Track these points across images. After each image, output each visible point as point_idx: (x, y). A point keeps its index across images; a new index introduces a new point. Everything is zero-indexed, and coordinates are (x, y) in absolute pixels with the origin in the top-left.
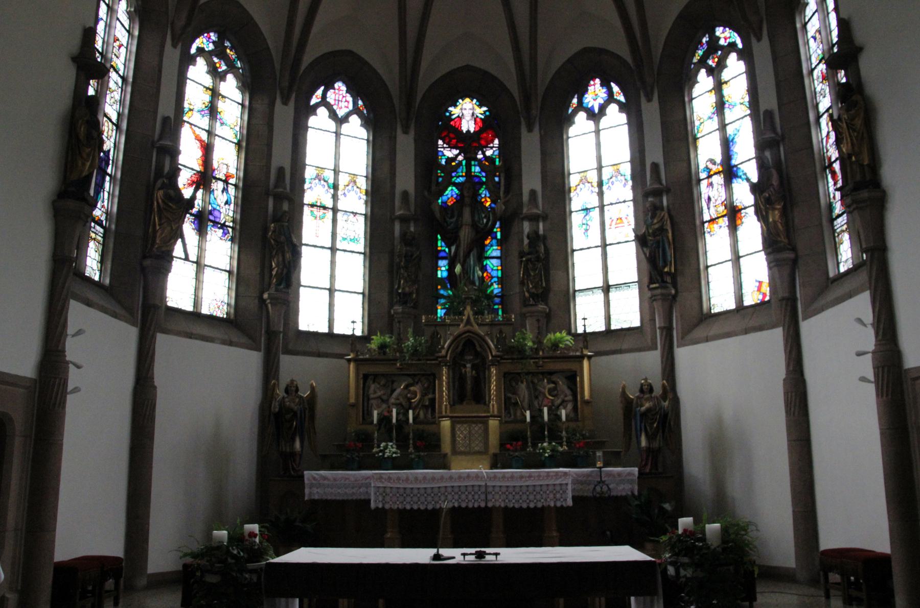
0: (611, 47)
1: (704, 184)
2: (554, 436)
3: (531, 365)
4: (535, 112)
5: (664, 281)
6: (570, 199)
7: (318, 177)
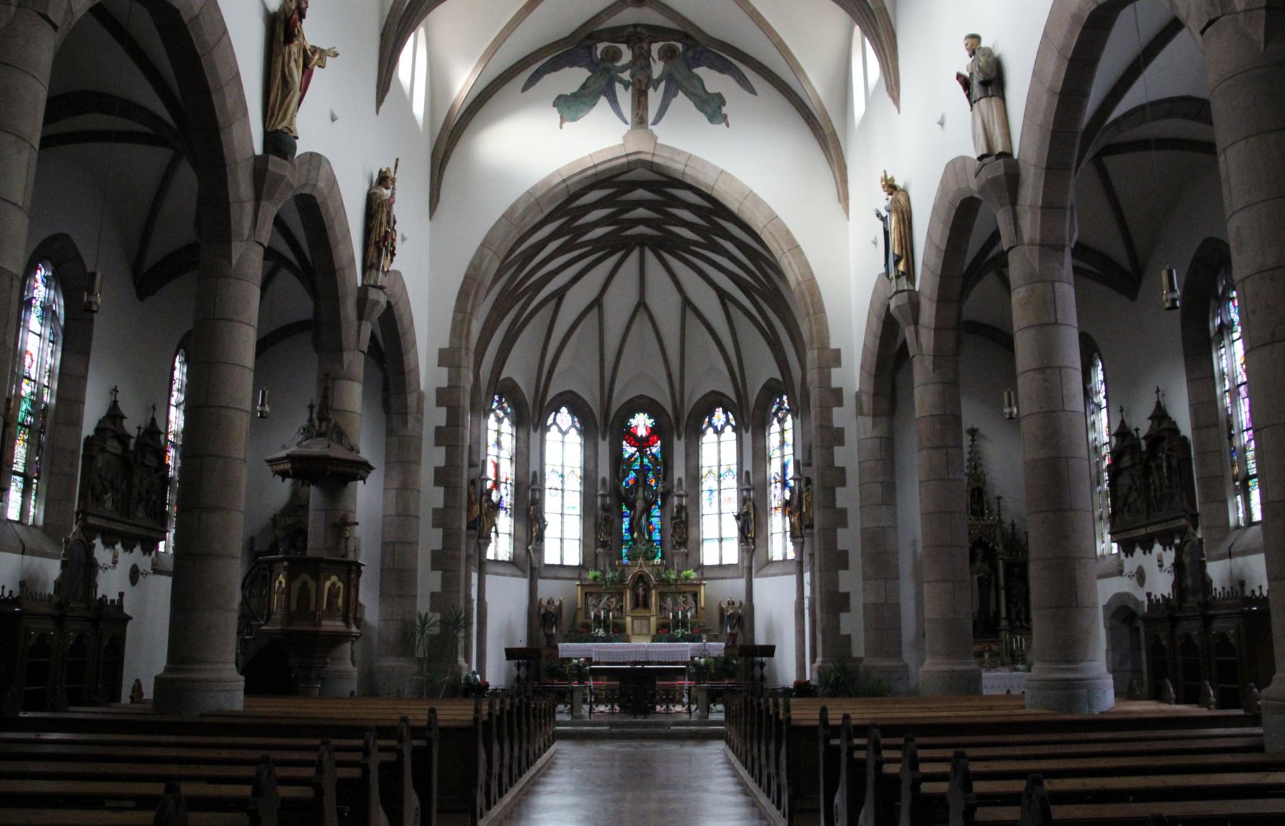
0: (727, 393)
2: (684, 625)
3: (673, 588)
4: (680, 425)
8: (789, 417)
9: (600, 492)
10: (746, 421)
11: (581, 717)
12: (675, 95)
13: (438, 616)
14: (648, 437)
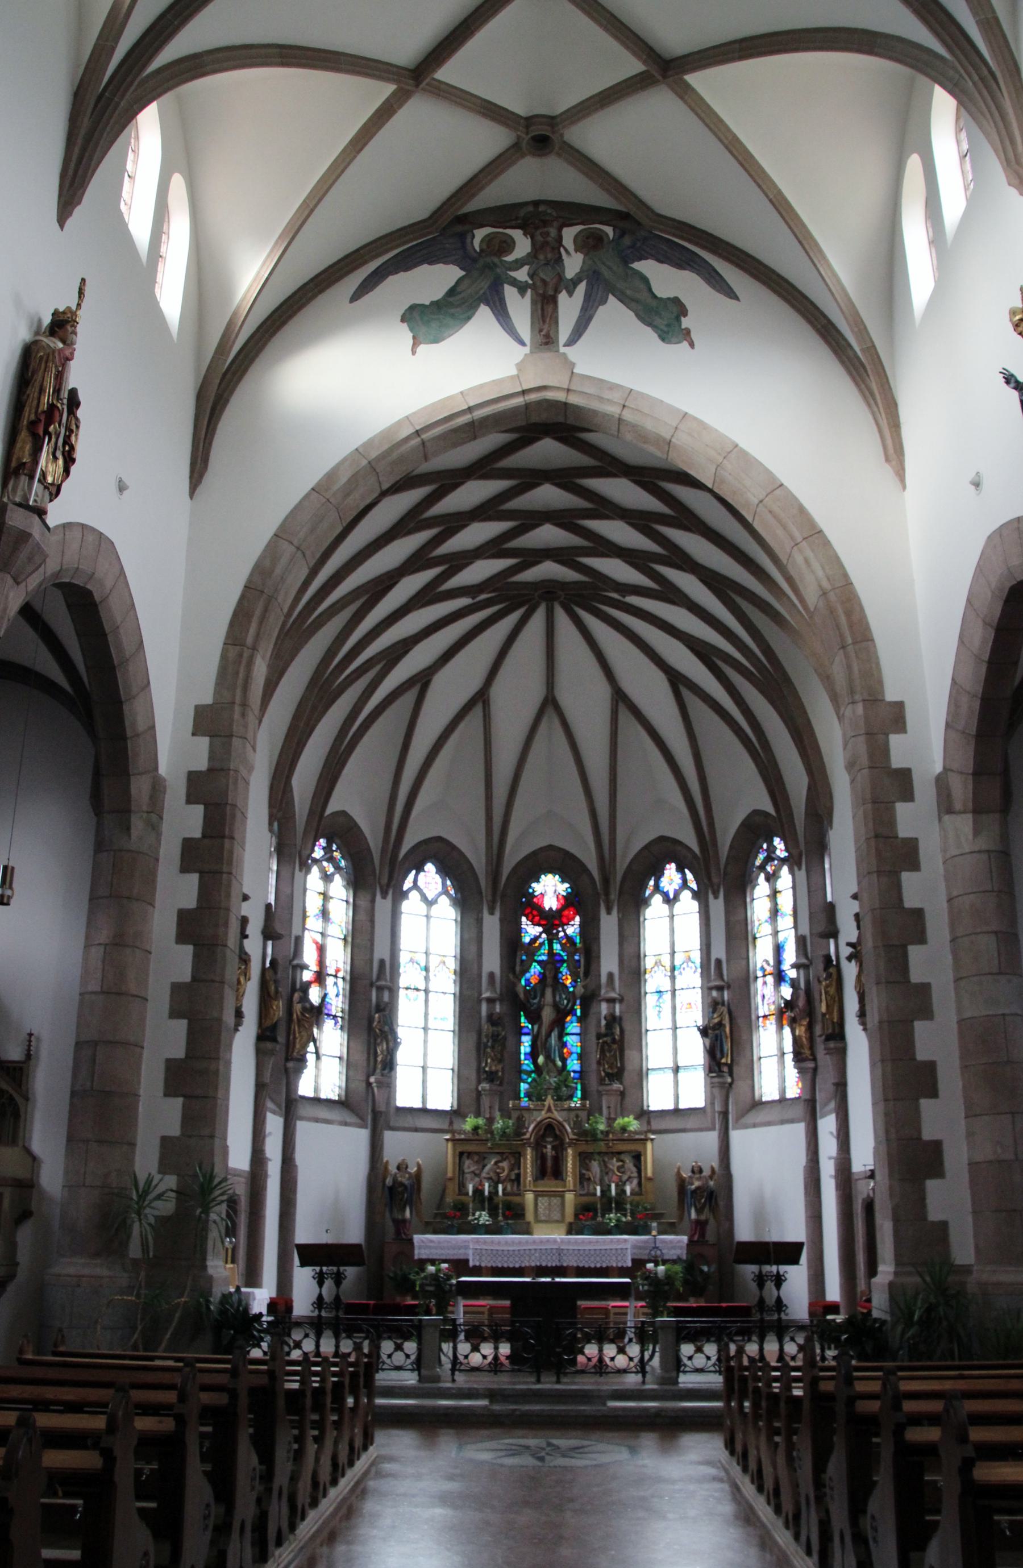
1: (760, 981)
2: (620, 1207)
3: (602, 1146)
4: (613, 890)
5: (721, 1071)
6: (645, 981)
7: (412, 960)
8: (785, 870)
9: (486, 995)
10: (715, 880)
11: (437, 1379)
12: (603, 301)
13: (171, 1181)
14: (560, 911)
